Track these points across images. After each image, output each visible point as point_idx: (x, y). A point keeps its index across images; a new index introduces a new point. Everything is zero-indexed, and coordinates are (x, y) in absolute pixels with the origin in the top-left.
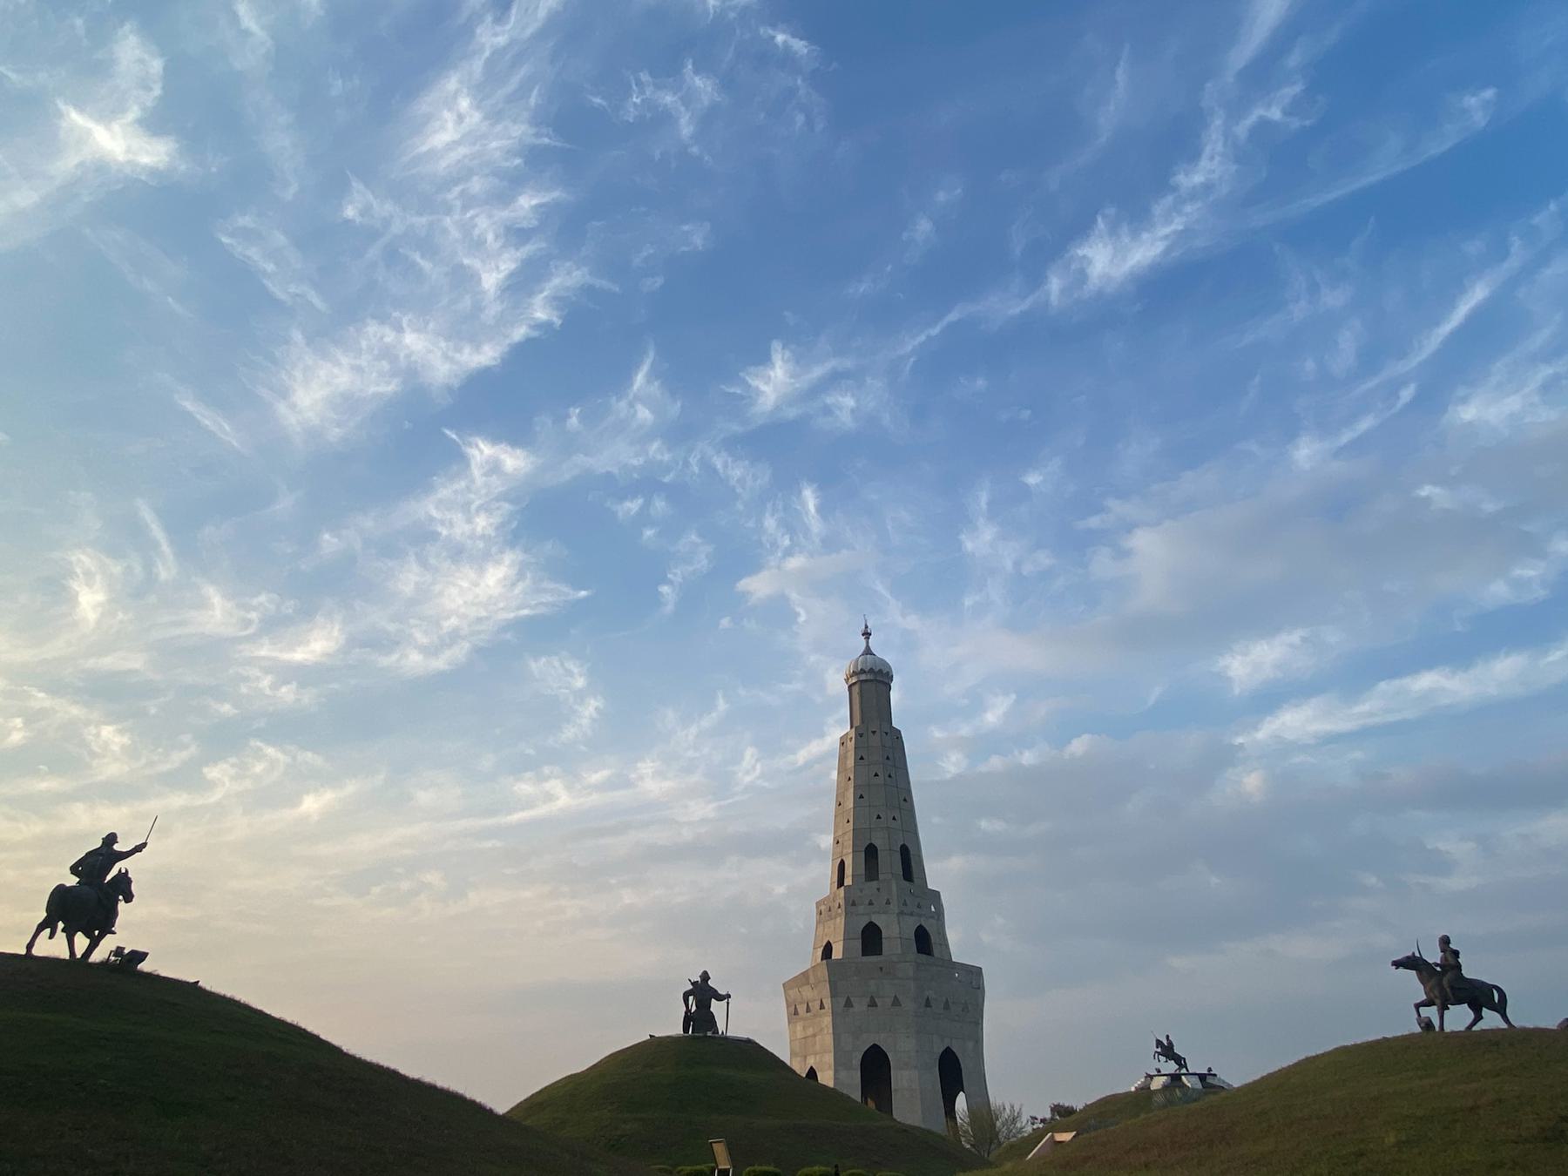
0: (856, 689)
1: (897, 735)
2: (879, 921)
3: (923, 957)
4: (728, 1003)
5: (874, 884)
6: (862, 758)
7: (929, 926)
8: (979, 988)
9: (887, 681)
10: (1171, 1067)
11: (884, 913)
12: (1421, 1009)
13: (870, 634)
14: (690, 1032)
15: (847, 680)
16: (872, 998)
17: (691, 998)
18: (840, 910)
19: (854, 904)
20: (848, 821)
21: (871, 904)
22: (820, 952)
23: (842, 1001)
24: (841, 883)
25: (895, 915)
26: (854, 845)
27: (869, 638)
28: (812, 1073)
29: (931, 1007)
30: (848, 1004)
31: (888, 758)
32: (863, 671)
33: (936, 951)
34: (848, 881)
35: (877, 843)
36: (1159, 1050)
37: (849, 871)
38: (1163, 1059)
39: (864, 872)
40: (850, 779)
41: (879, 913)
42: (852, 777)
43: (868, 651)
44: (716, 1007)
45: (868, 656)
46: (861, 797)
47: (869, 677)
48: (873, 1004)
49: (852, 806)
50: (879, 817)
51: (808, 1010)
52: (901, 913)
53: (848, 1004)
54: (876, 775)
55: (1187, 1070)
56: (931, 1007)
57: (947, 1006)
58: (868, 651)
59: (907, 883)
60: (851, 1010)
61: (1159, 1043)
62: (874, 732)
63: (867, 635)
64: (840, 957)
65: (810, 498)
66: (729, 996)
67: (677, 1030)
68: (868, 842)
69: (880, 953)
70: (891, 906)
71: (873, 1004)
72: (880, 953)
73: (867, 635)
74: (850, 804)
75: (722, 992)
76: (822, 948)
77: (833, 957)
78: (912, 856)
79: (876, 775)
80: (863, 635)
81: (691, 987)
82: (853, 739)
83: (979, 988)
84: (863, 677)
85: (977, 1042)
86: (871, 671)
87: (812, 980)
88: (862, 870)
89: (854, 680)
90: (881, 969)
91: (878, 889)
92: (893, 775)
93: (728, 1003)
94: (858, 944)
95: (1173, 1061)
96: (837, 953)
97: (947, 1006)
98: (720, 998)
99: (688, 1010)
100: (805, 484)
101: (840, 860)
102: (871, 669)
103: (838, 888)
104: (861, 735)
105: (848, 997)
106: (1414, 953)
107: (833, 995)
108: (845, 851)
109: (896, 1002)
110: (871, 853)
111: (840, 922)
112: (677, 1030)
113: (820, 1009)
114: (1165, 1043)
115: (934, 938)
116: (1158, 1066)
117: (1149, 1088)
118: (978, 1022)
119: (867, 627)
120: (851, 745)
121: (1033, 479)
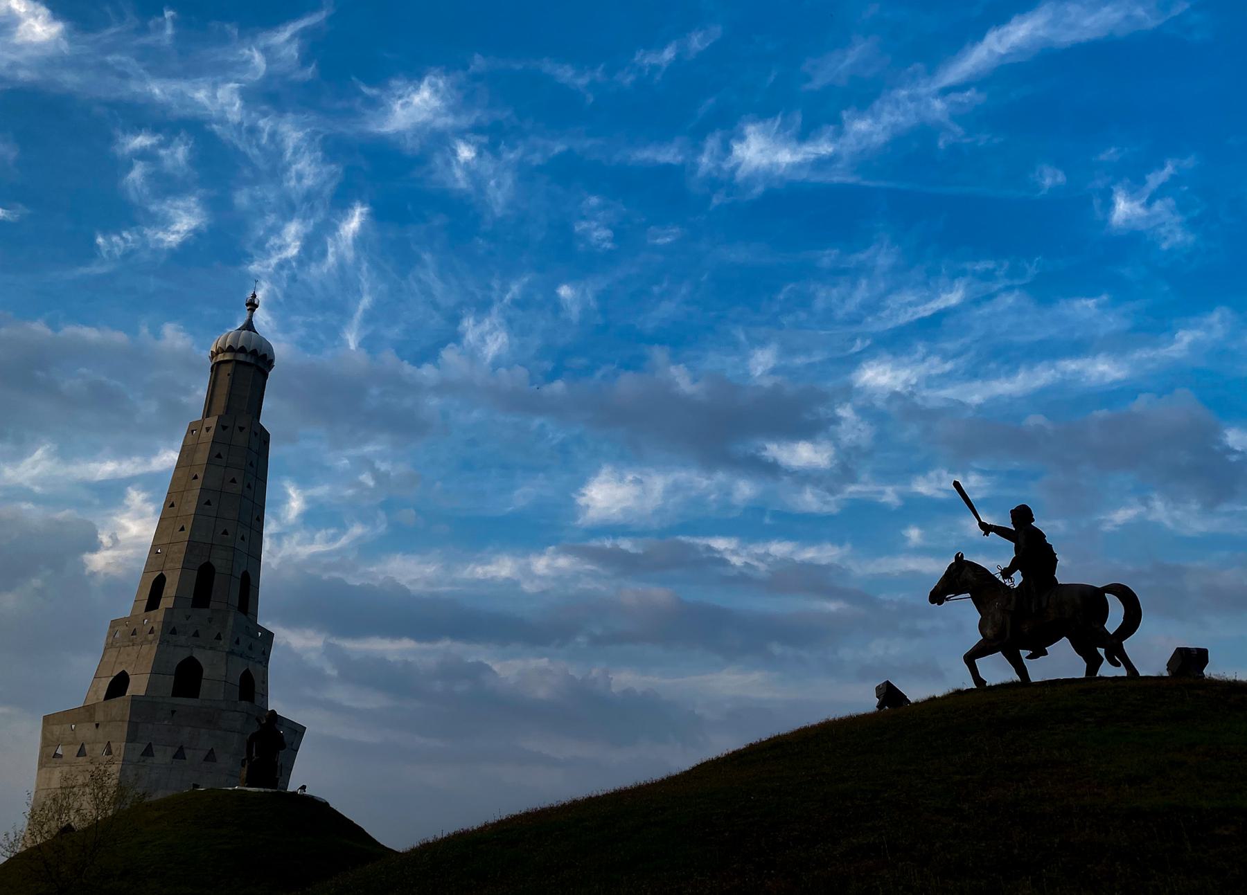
0: (227, 369)
1: (263, 438)
2: (201, 656)
6: (219, 456)
8: (295, 750)
11: (211, 648)
12: (979, 662)
13: (257, 306)
16: (181, 748)
18: (151, 637)
19: (174, 632)
20: (182, 529)
21: (196, 634)
22: (105, 684)
23: (141, 747)
24: (153, 603)
25: (224, 654)
26: (186, 560)
27: (254, 310)
28: (889, 694)
30: (148, 752)
31: (251, 464)
33: (258, 698)
34: (167, 602)
40: (196, 477)
41: (204, 648)
42: (201, 476)
46: (208, 503)
47: (228, 357)
48: (180, 754)
50: (225, 533)
52: (232, 653)
53: (148, 752)
54: (233, 481)
58: (249, 326)
60: (149, 760)
62: (241, 429)
65: (354, 222)
69: (197, 696)
70: (221, 643)
72: (197, 696)
74: (191, 508)
76: (111, 679)
79: (233, 481)
80: (247, 305)
84: (241, 357)
86: (254, 352)
87: (99, 717)
88: (190, 593)
94: (170, 680)
100: (363, 219)
101: (158, 573)
104: (224, 428)
105: (150, 744)
107: (132, 737)
108: (168, 566)
109: (210, 757)
111: (149, 651)
115: (258, 688)
119: (254, 296)
120: (207, 437)
121: (565, 291)
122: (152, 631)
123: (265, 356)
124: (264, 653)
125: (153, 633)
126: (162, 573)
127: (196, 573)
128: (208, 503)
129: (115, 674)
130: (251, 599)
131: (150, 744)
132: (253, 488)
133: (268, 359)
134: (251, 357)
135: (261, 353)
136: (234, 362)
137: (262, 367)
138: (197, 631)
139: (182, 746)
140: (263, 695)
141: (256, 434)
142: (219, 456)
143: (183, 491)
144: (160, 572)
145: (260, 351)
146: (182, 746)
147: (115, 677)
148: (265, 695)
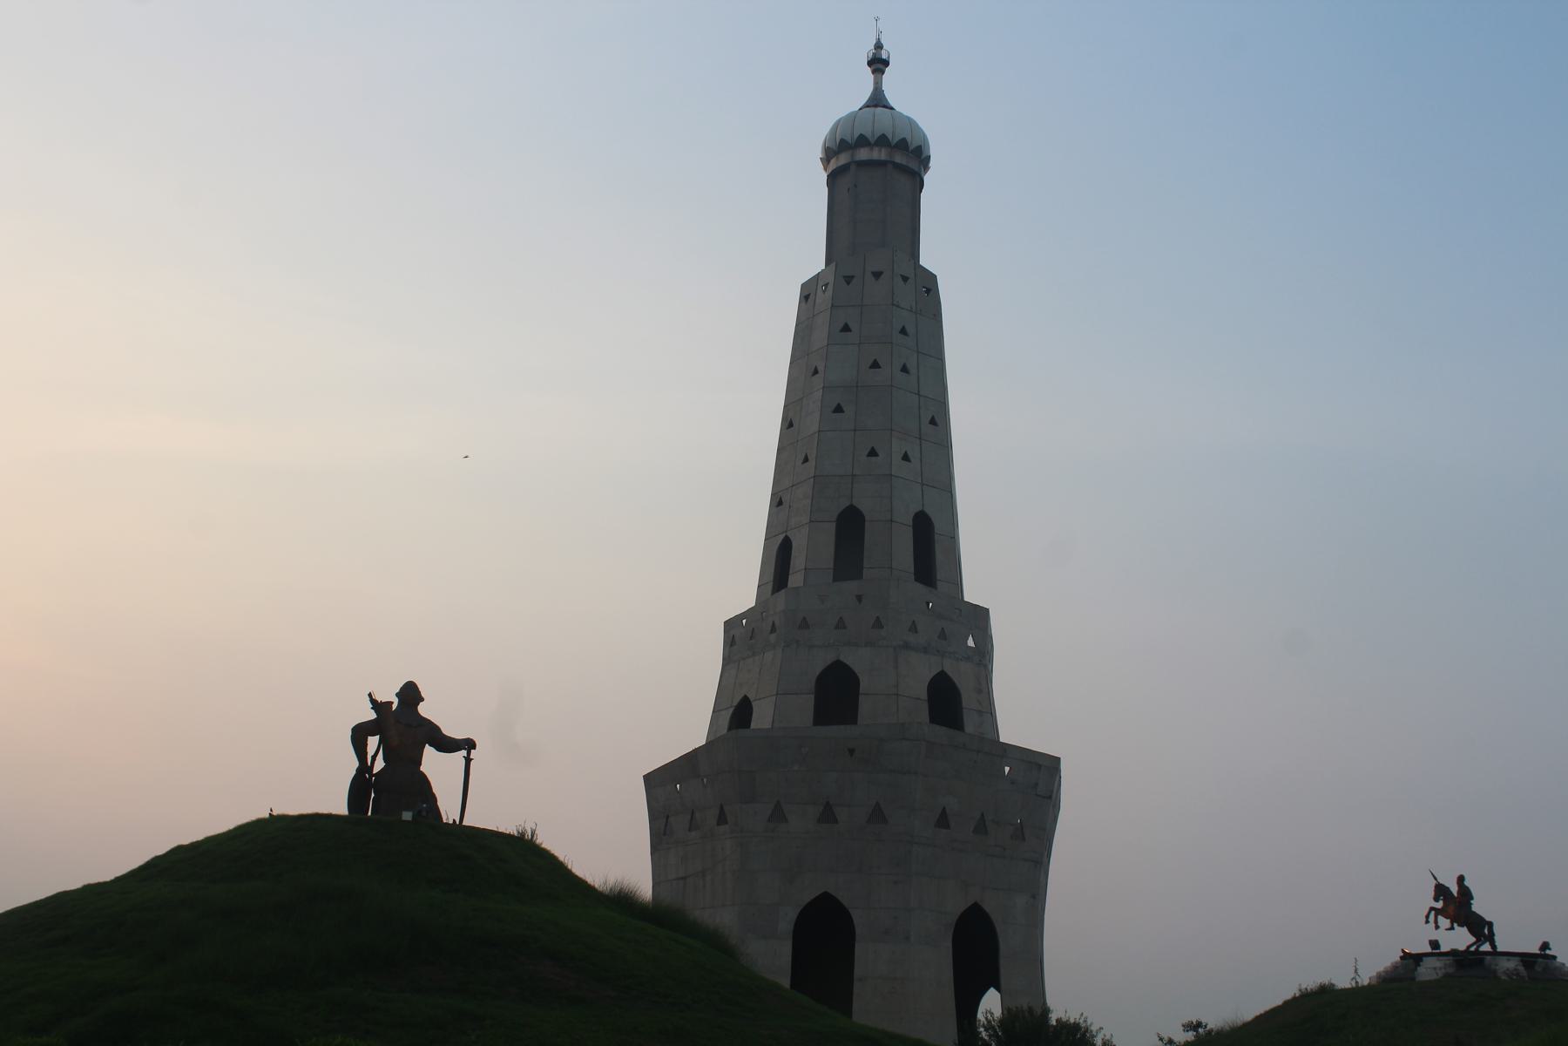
1: (928, 286)
2: (856, 659)
3: (941, 733)
4: (468, 760)
5: (851, 587)
6: (846, 329)
7: (962, 676)
9: (913, 165)
10: (1460, 939)
14: (370, 814)
15: (826, 160)
17: (373, 742)
18: (773, 637)
19: (804, 624)
20: (806, 460)
21: (841, 625)
29: (948, 827)
32: (862, 141)
33: (969, 727)
34: (795, 580)
35: (864, 505)
36: (1440, 905)
37: (798, 560)
38: (1444, 922)
39: (832, 566)
43: (877, 100)
44: (437, 767)
45: (879, 110)
46: (839, 409)
47: (879, 154)
48: (828, 815)
49: (815, 428)
51: (692, 826)
54: (875, 365)
55: (1493, 946)
56: (948, 827)
57: (981, 828)
58: (877, 100)
59: (920, 588)
61: (1441, 891)
62: (877, 275)
63: (878, 64)
64: (767, 725)
66: (469, 745)
67: (338, 805)
68: (844, 503)
71: (828, 815)
73: (878, 64)
75: (451, 730)
76: (731, 710)
77: (753, 725)
78: (936, 536)
81: (372, 715)
82: (830, 287)
83: (1050, 797)
84: (863, 154)
85: (1034, 897)
89: (843, 159)
90: (851, 751)
91: (859, 598)
92: (910, 329)
93: (468, 760)
95: (1465, 929)
96: (762, 718)
97: (981, 828)
98: (447, 745)
99: (364, 768)
101: (782, 537)
102: (842, 141)
103: (773, 593)
104: (848, 280)
106: (1550, 949)
110: (850, 525)
112: (338, 805)
113: (718, 824)
114: (1454, 889)
115: (968, 699)
116: (1435, 935)
117: (1413, 979)
118: (1039, 861)
119: (879, 46)
120: (823, 299)
122: (773, 629)
123: (904, 141)
124: (980, 691)
125: (775, 631)
126: (786, 536)
127: (833, 526)
128: (839, 409)
129: (735, 704)
130: (939, 556)
131: (778, 802)
132: (913, 371)
133: (924, 156)
134: (880, 151)
135: (897, 139)
136: (853, 167)
137: (904, 163)
138: (852, 755)
139: (828, 803)
140: (980, 713)
141: (905, 279)
142: (846, 329)
143: (801, 399)
144: (784, 535)
145: (894, 133)
146: (828, 803)
147: (736, 706)
148: (987, 710)
